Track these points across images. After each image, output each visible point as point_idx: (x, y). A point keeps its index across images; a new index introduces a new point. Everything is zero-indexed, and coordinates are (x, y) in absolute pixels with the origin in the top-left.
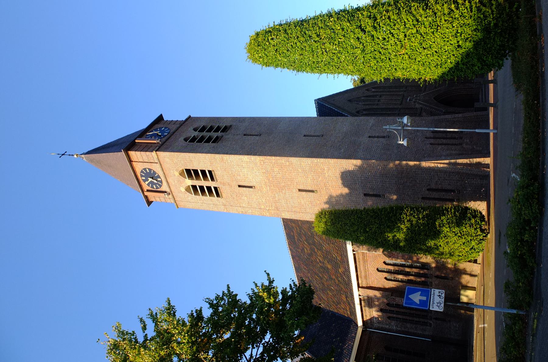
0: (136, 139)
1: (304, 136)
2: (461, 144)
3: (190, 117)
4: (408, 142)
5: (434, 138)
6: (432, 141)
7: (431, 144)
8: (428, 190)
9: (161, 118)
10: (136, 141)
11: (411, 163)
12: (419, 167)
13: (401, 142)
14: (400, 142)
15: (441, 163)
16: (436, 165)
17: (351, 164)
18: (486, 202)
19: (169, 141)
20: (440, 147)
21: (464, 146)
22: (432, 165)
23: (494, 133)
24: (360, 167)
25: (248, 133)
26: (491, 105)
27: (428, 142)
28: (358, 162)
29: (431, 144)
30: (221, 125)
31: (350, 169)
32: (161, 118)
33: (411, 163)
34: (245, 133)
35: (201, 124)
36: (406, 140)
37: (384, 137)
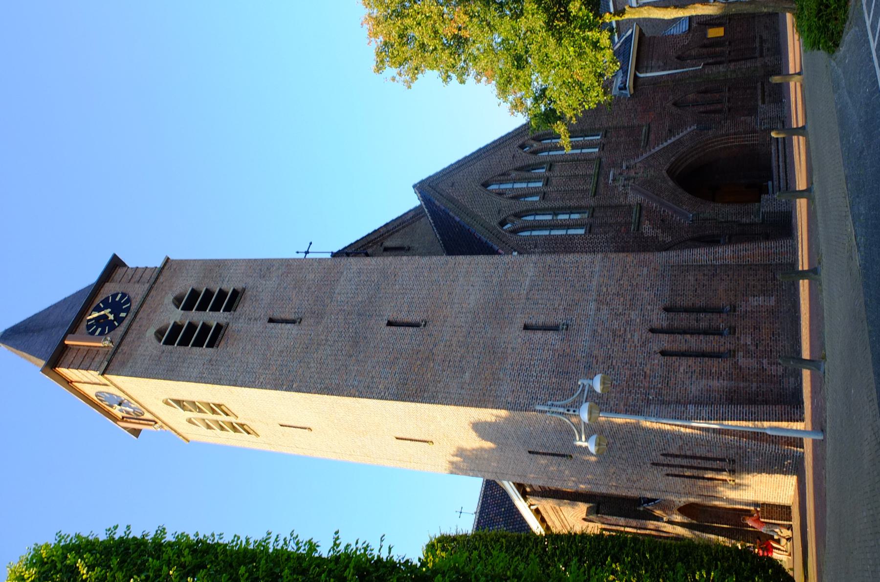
0: (64, 338)
1: (390, 324)
2: (732, 354)
3: (167, 260)
4: (598, 444)
5: (670, 331)
6: (665, 342)
7: (664, 353)
8: (663, 455)
9: (116, 263)
10: (66, 342)
11: (619, 420)
12: (637, 427)
13: (584, 444)
14: (578, 443)
15: (686, 427)
16: (677, 428)
17: (488, 415)
18: (795, 477)
19: (128, 339)
20: (684, 364)
21: (742, 361)
22: (668, 427)
23: (814, 441)
24: (506, 419)
25: (277, 315)
26: (803, 275)
27: (656, 348)
28: (503, 413)
29: (664, 353)
30: (224, 287)
31: (489, 420)
32: (116, 263)
33: (619, 420)
34: (271, 314)
35: (184, 285)
36: (594, 438)
37: (555, 328)
